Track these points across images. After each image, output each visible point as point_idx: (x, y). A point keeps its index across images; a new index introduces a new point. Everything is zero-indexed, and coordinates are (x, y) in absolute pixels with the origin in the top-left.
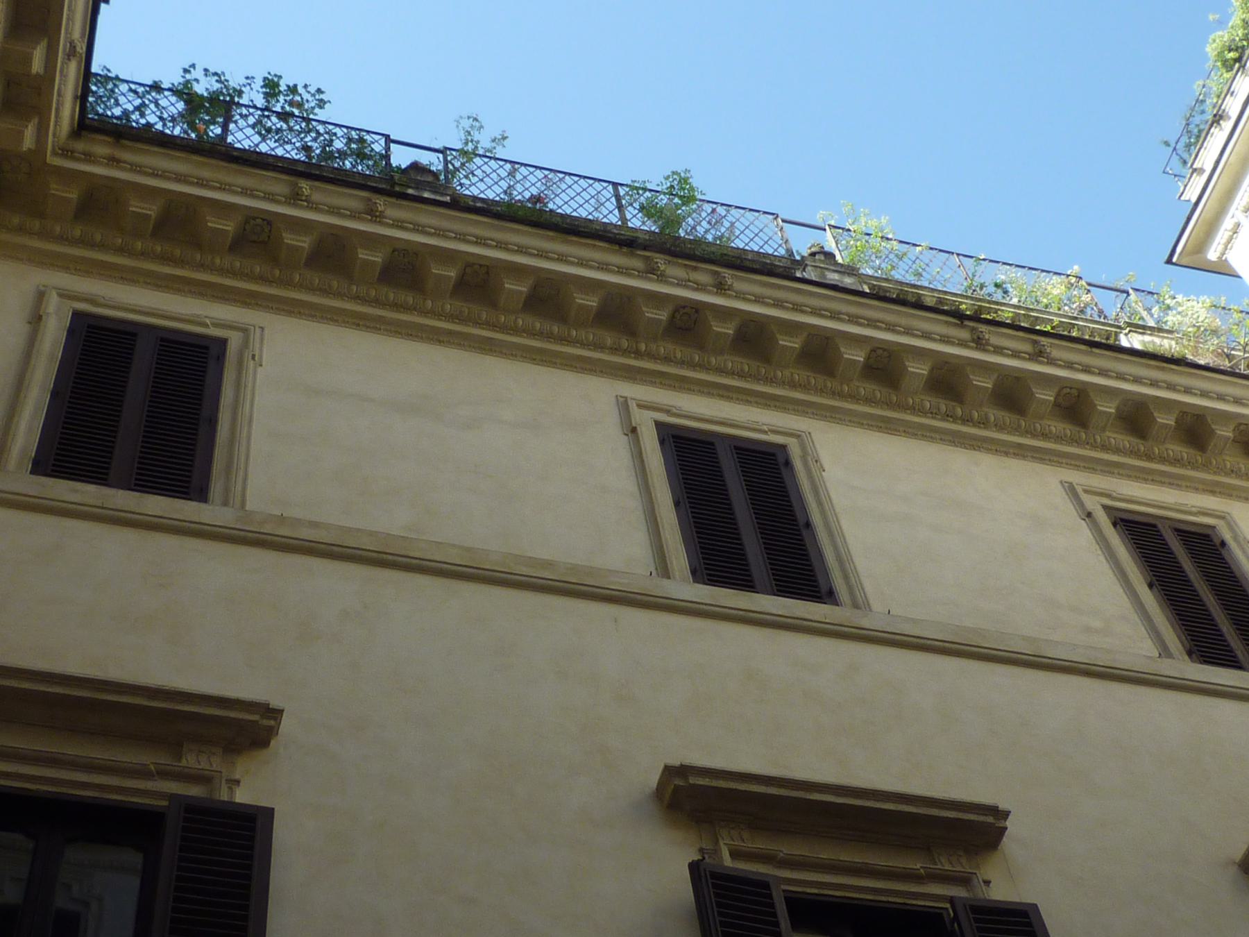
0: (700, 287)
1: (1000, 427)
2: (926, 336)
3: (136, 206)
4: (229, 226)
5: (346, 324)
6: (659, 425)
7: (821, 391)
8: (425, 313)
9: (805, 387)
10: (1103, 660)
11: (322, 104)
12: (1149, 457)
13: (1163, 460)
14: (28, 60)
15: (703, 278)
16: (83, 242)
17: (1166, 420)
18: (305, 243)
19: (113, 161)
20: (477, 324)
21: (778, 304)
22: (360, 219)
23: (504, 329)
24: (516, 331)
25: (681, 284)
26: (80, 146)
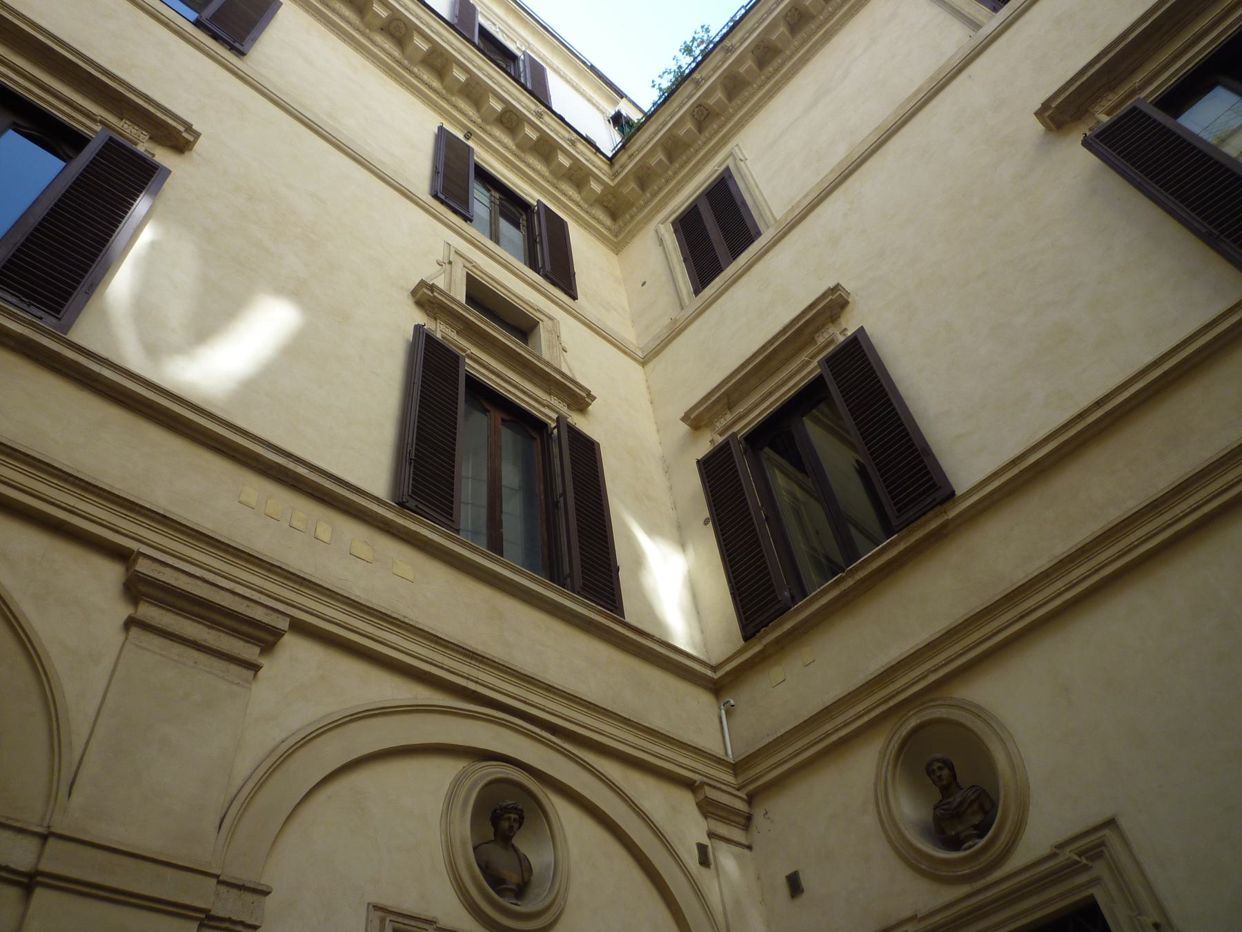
3: (653, 162)
4: (690, 125)
5: (766, 103)
8: (790, 57)
11: (707, 30)
14: (561, 165)
16: (654, 195)
18: (719, 95)
19: (631, 157)
20: (815, 33)
22: (727, 59)
23: (827, 20)
24: (832, 14)
26: (617, 166)
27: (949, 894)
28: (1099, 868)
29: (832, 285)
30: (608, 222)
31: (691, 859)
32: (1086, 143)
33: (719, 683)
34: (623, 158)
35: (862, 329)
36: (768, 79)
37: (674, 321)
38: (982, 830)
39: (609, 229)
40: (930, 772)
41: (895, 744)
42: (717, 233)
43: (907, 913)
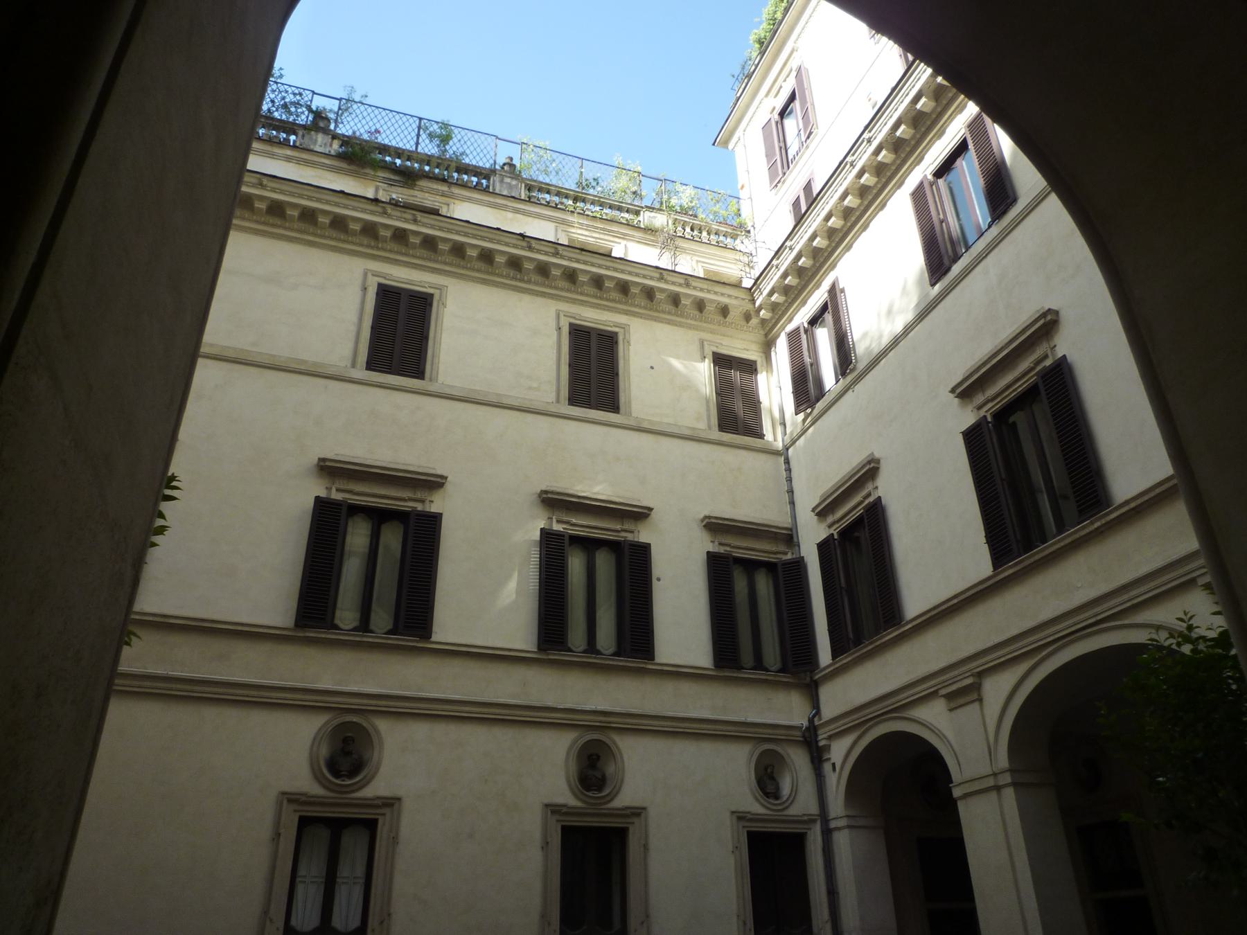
0: (406, 221)
1: (536, 284)
2: (507, 244)
6: (571, 325)
7: (458, 266)
8: (285, 228)
9: (451, 264)
10: (527, 404)
12: (601, 298)
13: (607, 300)
15: (409, 216)
17: (473, 253)
21: (441, 229)
25: (399, 219)
36: (265, 223)
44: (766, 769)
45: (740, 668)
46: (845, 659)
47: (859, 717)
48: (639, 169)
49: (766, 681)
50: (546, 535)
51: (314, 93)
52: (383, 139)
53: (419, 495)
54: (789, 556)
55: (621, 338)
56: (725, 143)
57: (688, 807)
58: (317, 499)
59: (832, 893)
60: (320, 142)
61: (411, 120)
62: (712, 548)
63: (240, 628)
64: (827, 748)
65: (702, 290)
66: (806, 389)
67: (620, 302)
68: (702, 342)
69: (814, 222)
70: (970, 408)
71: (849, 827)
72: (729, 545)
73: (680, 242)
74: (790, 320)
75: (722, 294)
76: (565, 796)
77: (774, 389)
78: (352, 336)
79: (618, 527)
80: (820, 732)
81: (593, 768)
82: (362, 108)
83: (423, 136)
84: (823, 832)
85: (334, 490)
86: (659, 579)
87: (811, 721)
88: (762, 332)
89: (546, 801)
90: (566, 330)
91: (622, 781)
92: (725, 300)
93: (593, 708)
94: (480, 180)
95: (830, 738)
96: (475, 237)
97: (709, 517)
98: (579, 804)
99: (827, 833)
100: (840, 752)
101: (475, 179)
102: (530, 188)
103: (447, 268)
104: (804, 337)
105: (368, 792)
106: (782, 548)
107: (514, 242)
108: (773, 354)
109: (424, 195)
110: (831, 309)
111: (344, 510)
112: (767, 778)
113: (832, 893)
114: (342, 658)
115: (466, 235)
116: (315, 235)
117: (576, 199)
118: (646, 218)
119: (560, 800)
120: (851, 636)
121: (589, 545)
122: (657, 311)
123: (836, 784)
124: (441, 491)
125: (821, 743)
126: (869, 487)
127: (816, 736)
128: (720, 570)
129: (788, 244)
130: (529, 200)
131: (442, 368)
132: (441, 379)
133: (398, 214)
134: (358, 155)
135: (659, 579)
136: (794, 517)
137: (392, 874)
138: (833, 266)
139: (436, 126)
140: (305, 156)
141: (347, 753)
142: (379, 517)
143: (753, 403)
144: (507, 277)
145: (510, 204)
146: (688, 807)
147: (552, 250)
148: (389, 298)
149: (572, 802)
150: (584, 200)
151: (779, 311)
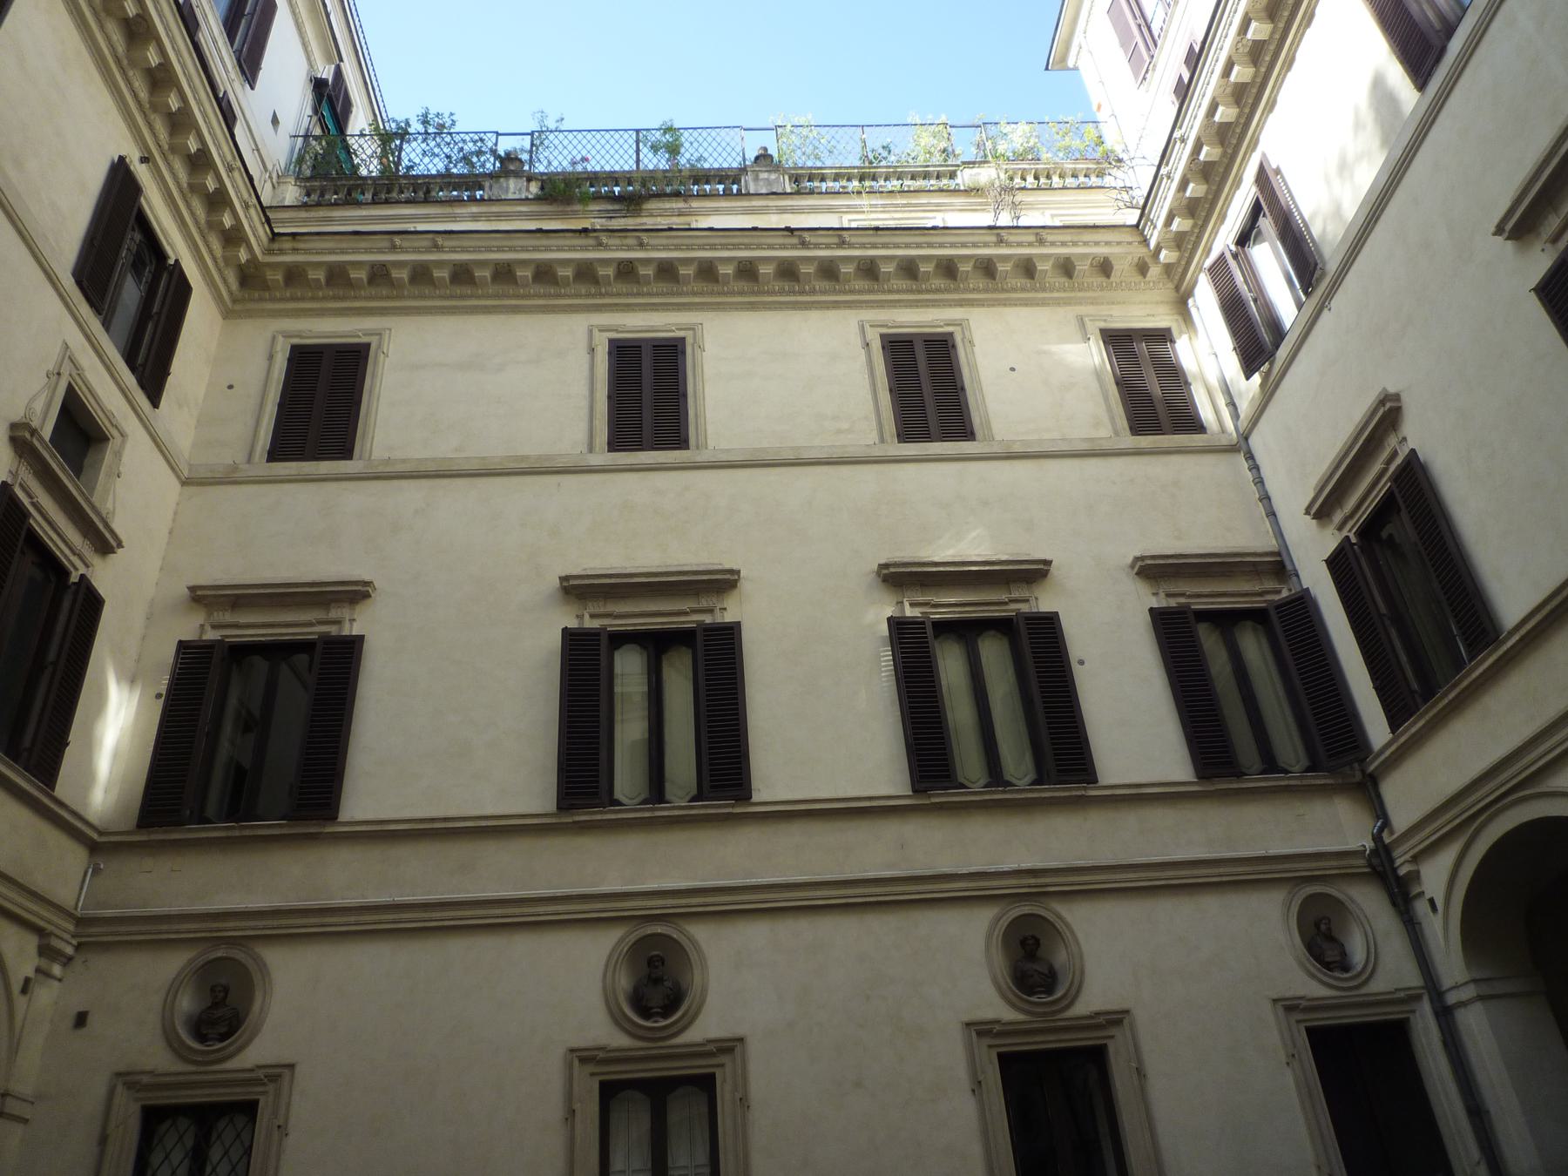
0: (630, 248)
2: (771, 247)
7: (712, 293)
8: (479, 297)
9: (701, 294)
10: (837, 453)
12: (920, 292)
16: (293, 299)
17: (727, 270)
21: (678, 248)
25: (619, 248)
26: (276, 246)
27: (180, 1067)
28: (271, 1088)
29: (367, 579)
30: (234, 286)
31: (16, 987)
32: (567, 633)
33: (99, 845)
34: (287, 244)
35: (361, 638)
36: (452, 297)
37: (235, 467)
38: (223, 1037)
39: (231, 293)
40: (212, 990)
41: (201, 961)
42: (320, 409)
43: (148, 1068)
44: (1317, 925)
45: (1239, 774)
46: (1415, 726)
47: (1456, 816)
48: (943, 119)
49: (1288, 790)
50: (899, 628)
51: (498, 134)
52: (593, 166)
53: (704, 603)
54: (1285, 593)
55: (958, 339)
56: (1063, 59)
57: (1199, 994)
58: (565, 630)
59: (1477, 1113)
60: (513, 188)
61: (626, 136)
62: (1154, 603)
63: (484, 823)
64: (1415, 876)
65: (1064, 244)
66: (1257, 342)
67: (947, 291)
68: (1081, 321)
69: (1209, 84)
70: (1538, 246)
71: (1480, 998)
72: (1182, 595)
73: (1020, 197)
74: (1208, 251)
75: (1097, 243)
76: (999, 1010)
77: (1206, 354)
78: (584, 413)
79: (1004, 597)
80: (1395, 854)
81: (1032, 959)
82: (561, 136)
83: (644, 150)
84: (1437, 1014)
85: (587, 617)
86: (1081, 662)
87: (1377, 838)
88: (1171, 286)
89: (967, 1018)
90: (876, 345)
91: (1082, 973)
92: (1103, 250)
93: (1014, 866)
94: (728, 181)
95: (1415, 859)
96: (725, 247)
97: (1142, 558)
98: (1021, 1017)
99: (1445, 1014)
100: (1437, 877)
101: (721, 187)
102: (796, 179)
103: (697, 300)
104: (1232, 263)
105: (695, 1034)
106: (1270, 584)
107: (781, 241)
108: (1193, 311)
109: (658, 215)
110: (1273, 212)
111: (604, 642)
112: (1322, 938)
113: (1477, 1113)
114: (632, 844)
115: (713, 247)
116: (518, 297)
117: (862, 179)
118: (965, 178)
119: (989, 1014)
120: (1415, 686)
121: (965, 631)
122: (1003, 290)
123: (1443, 933)
124: (735, 593)
125: (1402, 871)
126: (1392, 441)
127: (1392, 861)
128: (1173, 631)
129: (1177, 134)
130: (798, 193)
131: (710, 429)
132: (711, 443)
133: (617, 242)
134: (561, 191)
135: (1081, 662)
136: (1279, 534)
137: (746, 1156)
138: (1254, 143)
139: (658, 134)
140: (495, 209)
141: (657, 981)
142: (658, 644)
143: (1173, 374)
144: (782, 292)
145: (771, 203)
146: (1199, 994)
147: (836, 240)
148: (625, 354)
149: (1009, 1015)
150: (874, 178)
151: (1186, 244)
